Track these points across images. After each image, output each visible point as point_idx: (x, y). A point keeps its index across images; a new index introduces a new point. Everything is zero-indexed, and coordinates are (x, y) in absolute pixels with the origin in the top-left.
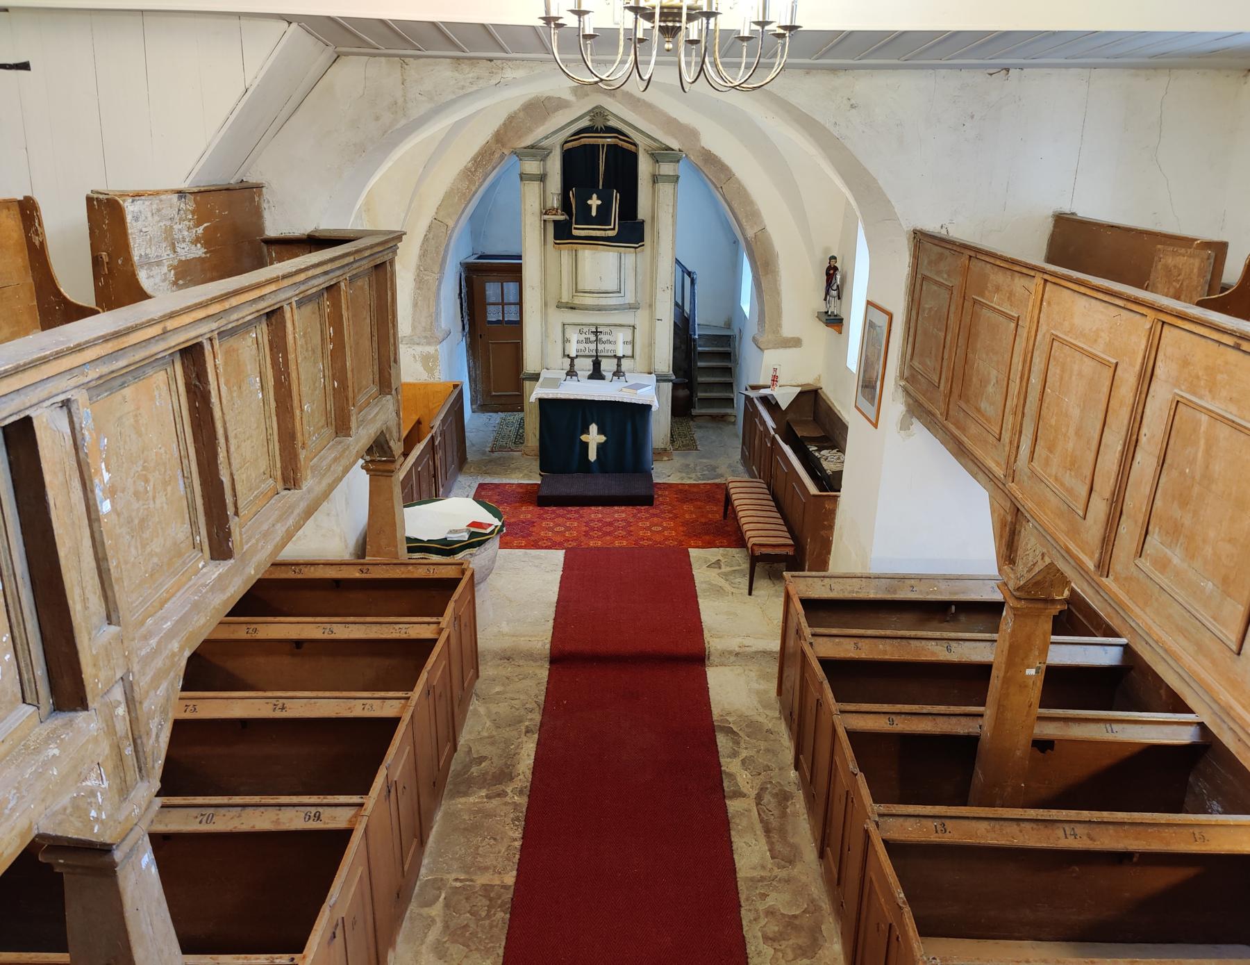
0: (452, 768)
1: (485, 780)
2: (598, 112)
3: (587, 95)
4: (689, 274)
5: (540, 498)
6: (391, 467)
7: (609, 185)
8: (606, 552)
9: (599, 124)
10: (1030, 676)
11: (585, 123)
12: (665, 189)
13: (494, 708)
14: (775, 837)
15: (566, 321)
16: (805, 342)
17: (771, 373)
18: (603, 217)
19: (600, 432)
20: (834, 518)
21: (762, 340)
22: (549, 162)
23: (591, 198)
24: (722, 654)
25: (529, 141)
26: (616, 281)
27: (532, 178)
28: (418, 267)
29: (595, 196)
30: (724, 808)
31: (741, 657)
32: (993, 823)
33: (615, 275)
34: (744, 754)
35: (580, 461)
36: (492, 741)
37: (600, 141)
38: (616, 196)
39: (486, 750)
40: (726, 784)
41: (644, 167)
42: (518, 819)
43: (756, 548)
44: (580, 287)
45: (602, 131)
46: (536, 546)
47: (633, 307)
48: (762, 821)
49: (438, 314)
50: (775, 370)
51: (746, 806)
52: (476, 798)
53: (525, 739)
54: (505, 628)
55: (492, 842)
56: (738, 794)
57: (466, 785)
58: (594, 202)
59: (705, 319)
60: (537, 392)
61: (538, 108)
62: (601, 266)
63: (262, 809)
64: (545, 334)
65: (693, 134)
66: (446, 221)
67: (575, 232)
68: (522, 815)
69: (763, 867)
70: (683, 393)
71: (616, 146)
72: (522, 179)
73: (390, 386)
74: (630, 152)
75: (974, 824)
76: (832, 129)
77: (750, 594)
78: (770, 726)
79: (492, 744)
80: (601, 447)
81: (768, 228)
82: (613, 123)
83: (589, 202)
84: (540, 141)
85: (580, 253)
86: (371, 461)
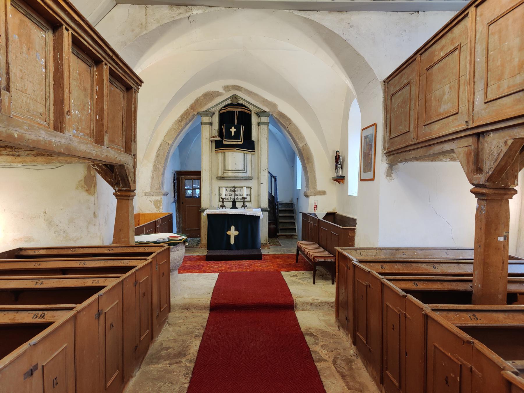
0: (150, 351)
1: (169, 357)
2: (234, 97)
3: (230, 90)
4: (274, 177)
5: (208, 258)
7: (239, 123)
8: (240, 273)
9: (235, 102)
10: (501, 242)
12: (263, 128)
13: (177, 328)
14: (349, 379)
15: (220, 186)
16: (327, 193)
17: (314, 204)
18: (237, 136)
19: (236, 230)
20: (354, 241)
21: (309, 192)
22: (214, 118)
23: (231, 128)
24: (303, 304)
25: (205, 108)
26: (243, 166)
27: (206, 124)
28: (155, 162)
29: (233, 127)
30: (315, 367)
31: (314, 305)
32: (507, 314)
33: (242, 163)
34: (322, 343)
35: (224, 238)
36: (175, 341)
37: (235, 110)
38: (242, 127)
39: (172, 345)
40: (313, 356)
41: (254, 120)
42: (188, 373)
43: (316, 258)
44: (227, 169)
45: (236, 105)
46: (204, 272)
47: (250, 178)
48: (338, 372)
49: (163, 183)
50: (315, 202)
51: (327, 365)
52: (162, 365)
53: (194, 339)
54: (186, 296)
55: (170, 384)
56: (321, 360)
57: (157, 358)
58: (233, 130)
59: (281, 198)
60: (204, 214)
61: (210, 96)
62: (236, 159)
63: (5, 312)
64: (211, 192)
65: (274, 106)
66: (168, 142)
67: (225, 143)
68: (190, 372)
70: (273, 226)
71: (242, 112)
73: (130, 151)
74: (248, 114)
75: (495, 315)
76: (342, 36)
77: (314, 283)
78: (334, 333)
79: (175, 342)
80: (236, 237)
81: (308, 144)
85: (227, 154)
86: (119, 191)
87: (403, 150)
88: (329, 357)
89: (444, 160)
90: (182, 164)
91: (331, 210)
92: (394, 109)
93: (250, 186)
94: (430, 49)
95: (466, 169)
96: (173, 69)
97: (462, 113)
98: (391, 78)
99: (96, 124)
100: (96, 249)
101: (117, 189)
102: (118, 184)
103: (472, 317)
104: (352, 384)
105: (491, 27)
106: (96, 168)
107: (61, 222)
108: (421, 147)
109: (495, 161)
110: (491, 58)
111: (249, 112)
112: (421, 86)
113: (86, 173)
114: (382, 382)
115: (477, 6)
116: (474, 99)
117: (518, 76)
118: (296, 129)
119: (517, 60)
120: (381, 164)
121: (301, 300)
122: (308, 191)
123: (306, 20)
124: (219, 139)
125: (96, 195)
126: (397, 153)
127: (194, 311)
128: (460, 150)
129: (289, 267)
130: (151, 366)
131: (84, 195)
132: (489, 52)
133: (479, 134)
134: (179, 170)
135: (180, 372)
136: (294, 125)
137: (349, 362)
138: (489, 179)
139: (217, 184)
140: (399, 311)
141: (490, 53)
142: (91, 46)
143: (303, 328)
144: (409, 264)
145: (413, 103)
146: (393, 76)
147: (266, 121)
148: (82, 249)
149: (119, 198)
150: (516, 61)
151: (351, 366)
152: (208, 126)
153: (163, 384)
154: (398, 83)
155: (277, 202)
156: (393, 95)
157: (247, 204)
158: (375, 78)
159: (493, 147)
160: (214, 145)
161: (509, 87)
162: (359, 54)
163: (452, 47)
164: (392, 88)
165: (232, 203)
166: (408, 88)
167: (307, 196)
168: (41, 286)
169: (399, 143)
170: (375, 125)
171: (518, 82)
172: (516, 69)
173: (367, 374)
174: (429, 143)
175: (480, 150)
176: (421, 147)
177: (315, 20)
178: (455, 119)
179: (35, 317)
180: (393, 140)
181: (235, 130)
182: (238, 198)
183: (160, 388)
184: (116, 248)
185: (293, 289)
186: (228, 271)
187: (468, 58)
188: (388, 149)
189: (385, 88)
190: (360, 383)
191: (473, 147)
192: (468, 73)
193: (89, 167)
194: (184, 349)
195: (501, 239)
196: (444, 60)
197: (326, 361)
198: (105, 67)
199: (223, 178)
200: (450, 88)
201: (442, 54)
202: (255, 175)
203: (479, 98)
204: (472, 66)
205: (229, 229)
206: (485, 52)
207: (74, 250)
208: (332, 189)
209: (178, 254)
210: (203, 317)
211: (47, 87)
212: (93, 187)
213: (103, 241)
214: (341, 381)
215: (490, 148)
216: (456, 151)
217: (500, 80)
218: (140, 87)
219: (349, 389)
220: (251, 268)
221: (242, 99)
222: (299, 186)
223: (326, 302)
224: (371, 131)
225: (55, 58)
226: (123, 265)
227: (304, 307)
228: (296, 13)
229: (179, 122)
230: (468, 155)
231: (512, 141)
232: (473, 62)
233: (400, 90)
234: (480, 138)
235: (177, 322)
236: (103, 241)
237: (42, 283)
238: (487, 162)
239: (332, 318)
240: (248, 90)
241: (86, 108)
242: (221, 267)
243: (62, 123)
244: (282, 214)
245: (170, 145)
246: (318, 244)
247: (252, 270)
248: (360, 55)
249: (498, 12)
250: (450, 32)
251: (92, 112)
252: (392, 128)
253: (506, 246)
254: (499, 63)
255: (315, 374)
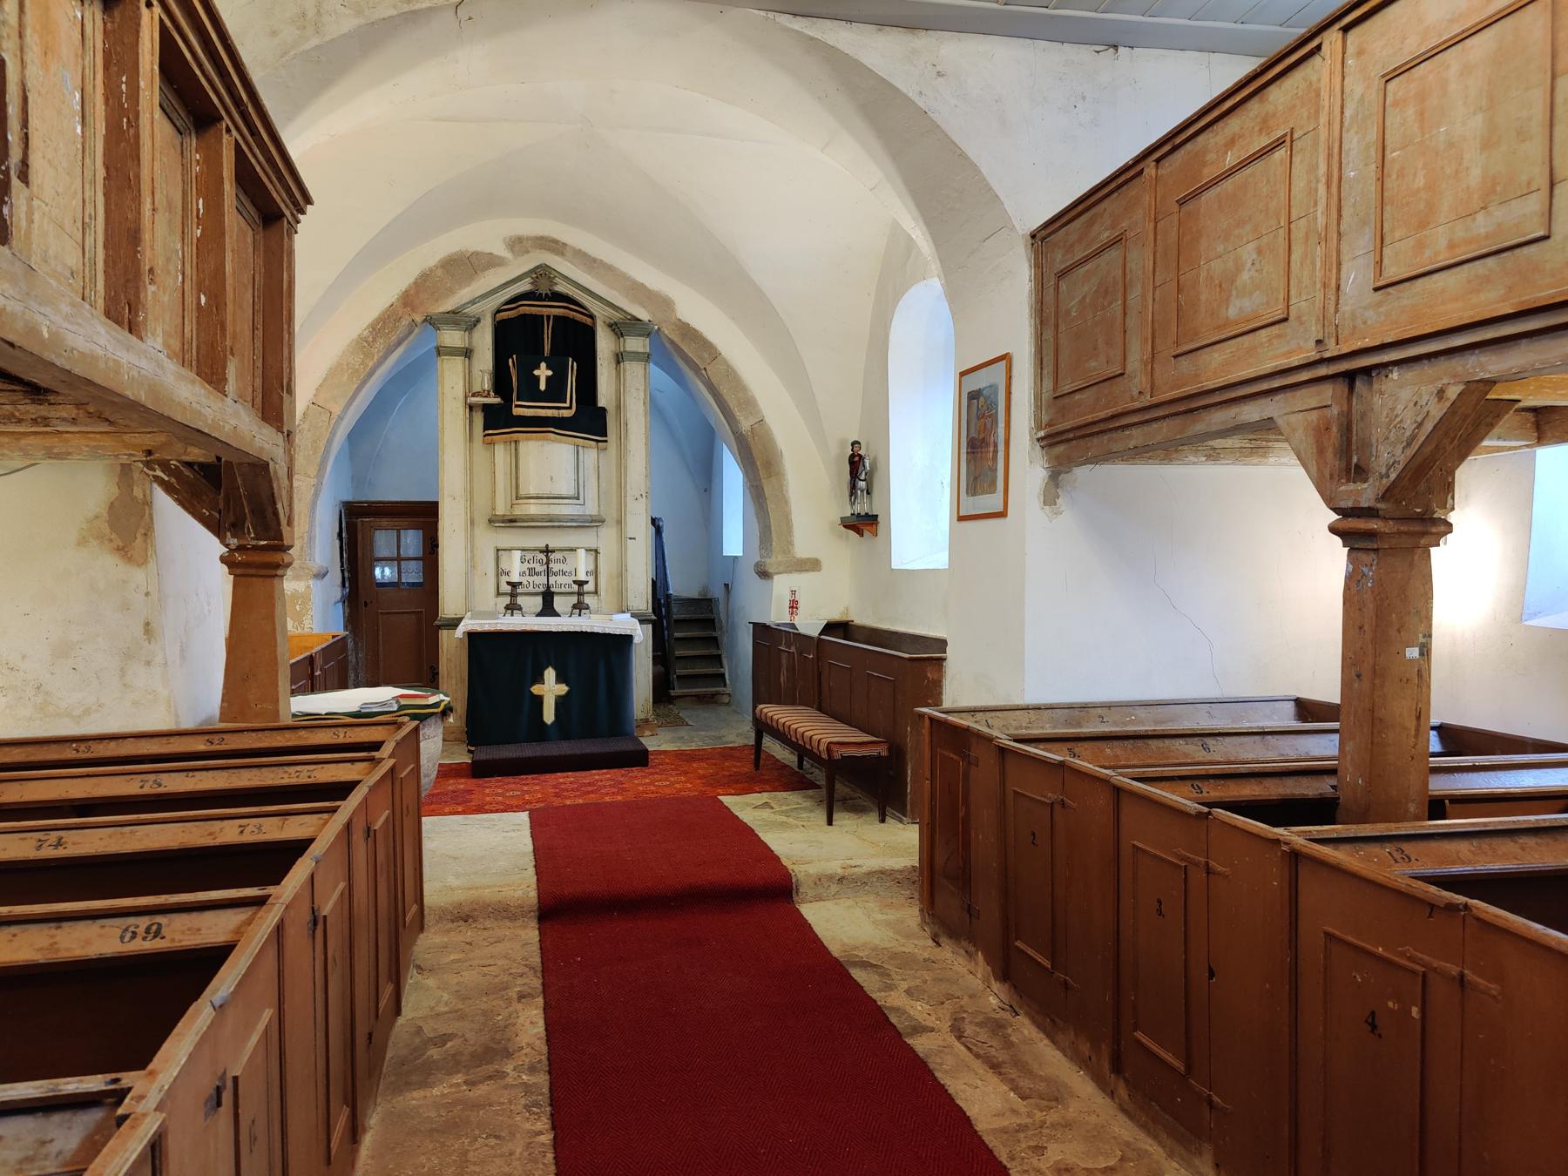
1: (458, 1063)
5: (479, 770)
6: (276, 557)
9: (542, 287)
11: (524, 286)
14: (1013, 1073)
15: (501, 546)
16: (825, 564)
18: (555, 391)
19: (560, 679)
21: (771, 564)
22: (477, 333)
23: (538, 367)
24: (819, 880)
25: (449, 305)
26: (573, 484)
27: (453, 352)
29: (543, 365)
31: (847, 883)
32: (1475, 842)
33: (572, 475)
34: (904, 985)
35: (533, 706)
37: (545, 311)
38: (572, 367)
40: (894, 1020)
41: (605, 344)
42: (536, 1104)
43: (835, 748)
44: (522, 492)
45: (548, 298)
46: (480, 810)
47: (595, 522)
48: (977, 1056)
50: (794, 593)
53: (519, 1006)
54: (453, 881)
55: (492, 1141)
56: (919, 1029)
57: (419, 1072)
58: (543, 372)
61: (463, 265)
62: (550, 462)
63: (14, 929)
65: (666, 303)
66: (328, 406)
67: (516, 411)
69: (1014, 1112)
72: (439, 354)
74: (585, 325)
76: (916, 99)
77: (830, 822)
78: (926, 955)
80: (561, 702)
81: (767, 420)
82: (562, 288)
83: (536, 372)
84: (465, 305)
85: (523, 446)
86: (240, 548)
87: (1102, 426)
88: (938, 1019)
89: (1192, 459)
90: (357, 480)
91: (836, 615)
92: (1068, 312)
93: (594, 546)
94: (1188, 146)
95: (1314, 470)
96: (394, 173)
97: (1299, 318)
98: (1058, 224)
99: (198, 323)
100: (164, 740)
101: (234, 542)
102: (237, 528)
103: (1395, 854)
104: (1025, 1083)
105: (1392, 86)
106: (159, 473)
107: (24, 657)
108: (1164, 417)
109: (1409, 444)
110: (1392, 170)
111: (588, 321)
112: (1160, 249)
113: (115, 491)
114: (1117, 1068)
115: (1346, 30)
116: (1338, 279)
117: (1480, 217)
118: (731, 374)
119: (1476, 172)
120: (1026, 465)
121: (812, 870)
122: (768, 561)
123: (815, 45)
124: (498, 400)
125: (152, 565)
126: (1075, 438)
127: (488, 924)
128: (1293, 418)
129: (737, 782)
130: (408, 1095)
131: (107, 565)
132: (1388, 152)
133: (1355, 373)
134: (350, 499)
135: (510, 1102)
136: (725, 362)
137: (997, 1027)
138: (1386, 495)
139: (489, 540)
140: (1183, 859)
141: (1390, 156)
142: (200, 66)
143: (835, 950)
144: (1140, 743)
145: (1134, 295)
146: (1064, 220)
147: (641, 350)
148: (113, 744)
149: (239, 571)
150: (1475, 176)
151: (1006, 1037)
152: (459, 362)
153: (471, 1144)
154: (1080, 240)
155: (668, 596)
156: (1062, 275)
157: (588, 600)
158: (1007, 225)
159: (1400, 407)
160: (479, 419)
161: (1451, 246)
162: (963, 155)
163: (1265, 141)
164: (1059, 256)
165: (539, 600)
166: (1114, 254)
167: (764, 574)
168: (60, 853)
169: (1089, 408)
170: (1006, 358)
171: (1482, 230)
172: (1476, 196)
173: (1058, 1054)
174: (1192, 404)
175: (1355, 417)
176: (1164, 417)
177: (840, 46)
178: (1279, 336)
179: (129, 935)
180: (1066, 400)
181: (550, 373)
182: (560, 582)
183: (466, 1153)
184: (236, 736)
185: (776, 841)
186: (557, 802)
187: (1322, 169)
188: (1049, 425)
189: (1036, 253)
190: (1047, 1079)
191: (1335, 410)
192: (1321, 208)
193: (126, 470)
194: (498, 1036)
195: (1413, 653)
196: (1238, 176)
197: (932, 1030)
198: (225, 136)
199: (511, 522)
200: (1259, 251)
201: (1230, 160)
202: (610, 514)
203: (1356, 277)
204: (1334, 189)
205: (540, 679)
206: (1373, 153)
207: (83, 747)
208: (839, 553)
209: (433, 747)
210: (524, 941)
211: (87, 186)
212: (140, 539)
213: (177, 715)
214: (993, 1079)
215: (1392, 409)
216: (1280, 422)
217: (1423, 224)
218: (301, 217)
219: (1023, 1098)
220: (624, 789)
221: (566, 278)
222: (733, 543)
223: (882, 872)
224: (997, 374)
225: (111, 94)
226: (294, 781)
227: (822, 890)
228: (785, 20)
229: (364, 344)
230: (1321, 431)
231: (1461, 387)
232: (1336, 181)
233: (1086, 260)
234: (1358, 384)
235: (447, 960)
236: (177, 715)
237: (59, 843)
238: (1381, 448)
239: (911, 915)
240: (585, 254)
241: (171, 268)
242: (527, 792)
243: (134, 306)
244: (688, 626)
245: (335, 417)
246: (820, 709)
247: (630, 796)
248: (967, 158)
249: (1414, 46)
250: (1256, 99)
251: (188, 282)
252: (1062, 365)
253: (1425, 674)
254: (1420, 182)
255: (919, 1070)
